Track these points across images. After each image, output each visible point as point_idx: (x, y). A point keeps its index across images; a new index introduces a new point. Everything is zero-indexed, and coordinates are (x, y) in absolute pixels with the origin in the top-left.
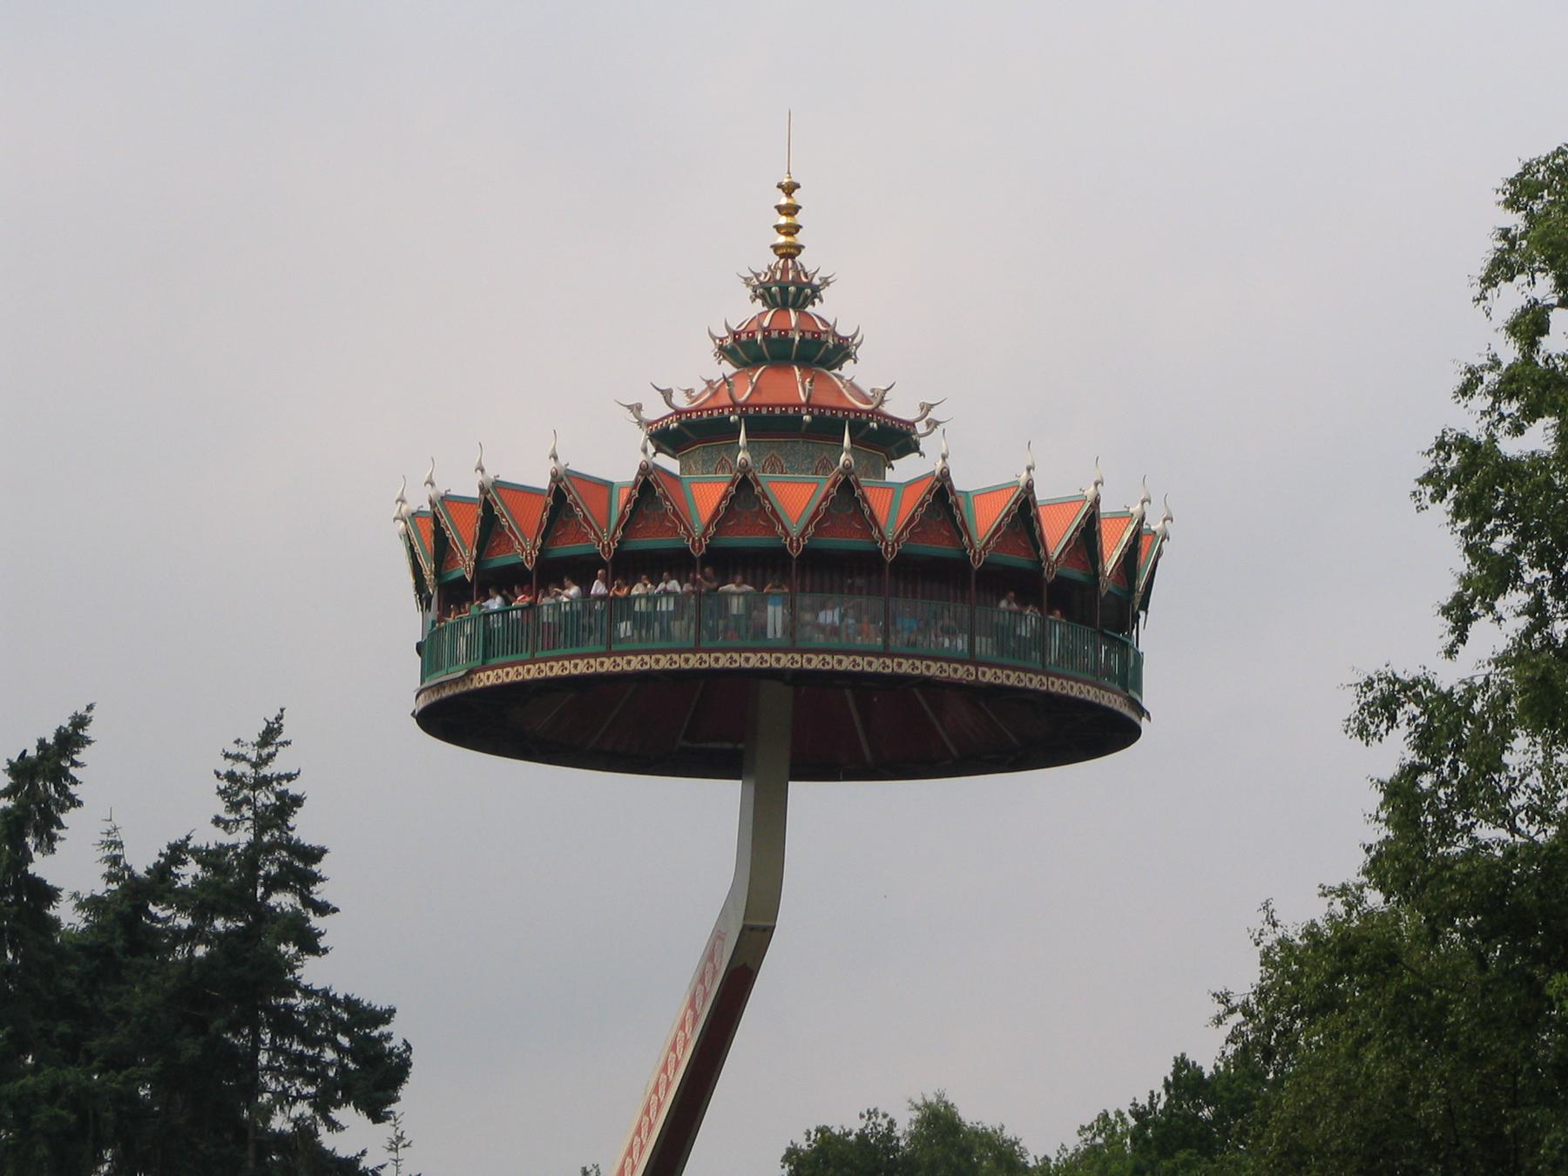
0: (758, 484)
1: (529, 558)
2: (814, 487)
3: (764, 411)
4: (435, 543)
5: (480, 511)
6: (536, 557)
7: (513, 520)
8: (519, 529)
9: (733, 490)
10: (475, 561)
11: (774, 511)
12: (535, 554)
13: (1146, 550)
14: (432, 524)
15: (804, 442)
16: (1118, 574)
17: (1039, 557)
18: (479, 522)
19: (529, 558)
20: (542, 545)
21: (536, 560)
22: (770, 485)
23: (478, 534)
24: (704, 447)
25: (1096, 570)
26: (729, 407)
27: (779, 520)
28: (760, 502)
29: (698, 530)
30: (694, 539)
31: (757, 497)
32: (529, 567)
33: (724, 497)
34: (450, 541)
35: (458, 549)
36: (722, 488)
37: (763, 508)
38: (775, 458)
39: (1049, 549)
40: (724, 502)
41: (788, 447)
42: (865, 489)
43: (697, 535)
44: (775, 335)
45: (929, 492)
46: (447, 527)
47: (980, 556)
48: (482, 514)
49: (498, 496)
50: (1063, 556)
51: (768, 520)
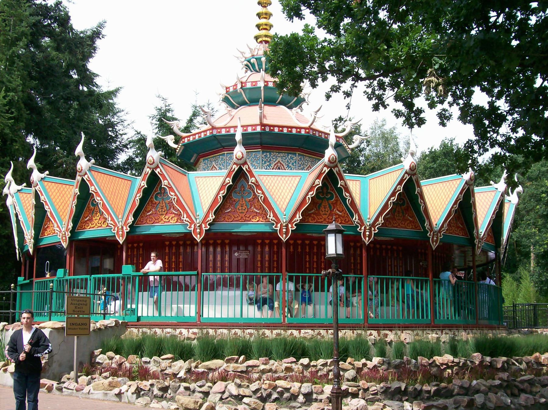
0: (252, 176)
1: (120, 233)
2: (298, 179)
3: (276, 130)
4: (35, 215)
5: (77, 191)
6: (69, 238)
7: (106, 198)
8: (110, 206)
9: (229, 181)
10: (71, 232)
11: (266, 200)
12: (126, 229)
13: (482, 219)
14: (34, 200)
15: (299, 154)
16: (488, 235)
17: (424, 228)
18: (76, 200)
19: (120, 233)
20: (133, 222)
21: (127, 235)
22: (261, 178)
23: (74, 210)
24: (227, 153)
25: (472, 234)
26: (209, 130)
27: (271, 208)
28: (254, 192)
29: (201, 214)
30: (118, 227)
31: (251, 187)
32: (121, 241)
33: (222, 188)
34: (100, 207)
35: (55, 221)
36: (219, 182)
37: (256, 197)
38: (280, 163)
39: (433, 220)
40: (222, 192)
41: (289, 157)
42: (348, 182)
43: (198, 221)
44: (249, 85)
45: (400, 183)
46: (45, 202)
47: (370, 232)
48: (35, 203)
49: (93, 176)
50: (445, 226)
51: (261, 208)
